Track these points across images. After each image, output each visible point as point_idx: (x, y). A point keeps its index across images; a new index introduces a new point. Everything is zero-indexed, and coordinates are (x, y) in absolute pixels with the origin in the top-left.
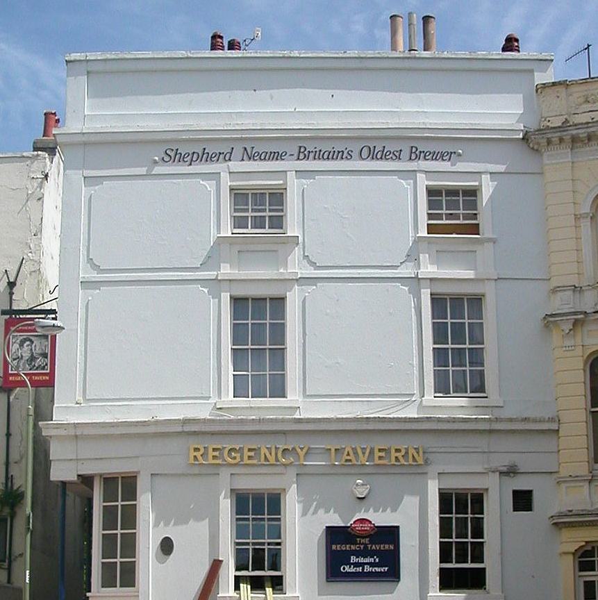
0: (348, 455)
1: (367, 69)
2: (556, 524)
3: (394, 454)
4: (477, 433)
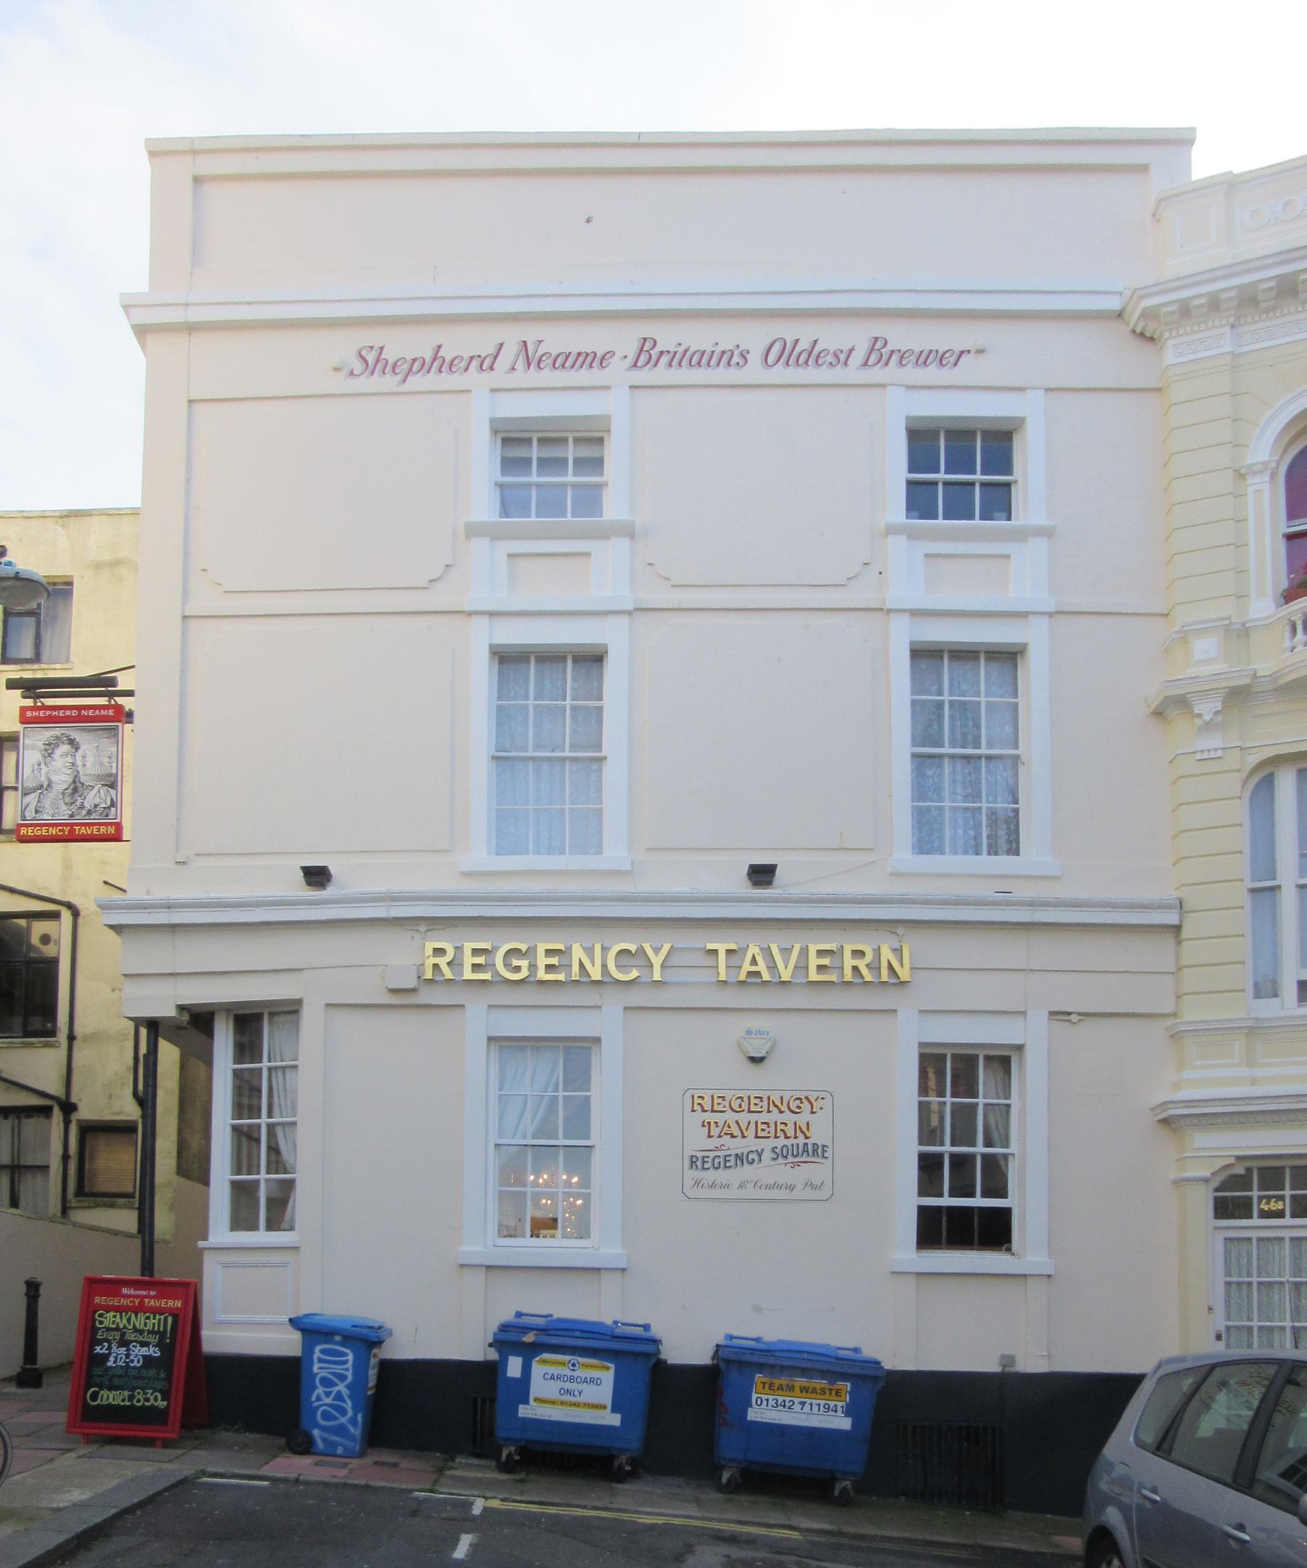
0: (754, 962)
1: (248, 150)
2: (1165, 1122)
3: (849, 962)
4: (523, 1048)
